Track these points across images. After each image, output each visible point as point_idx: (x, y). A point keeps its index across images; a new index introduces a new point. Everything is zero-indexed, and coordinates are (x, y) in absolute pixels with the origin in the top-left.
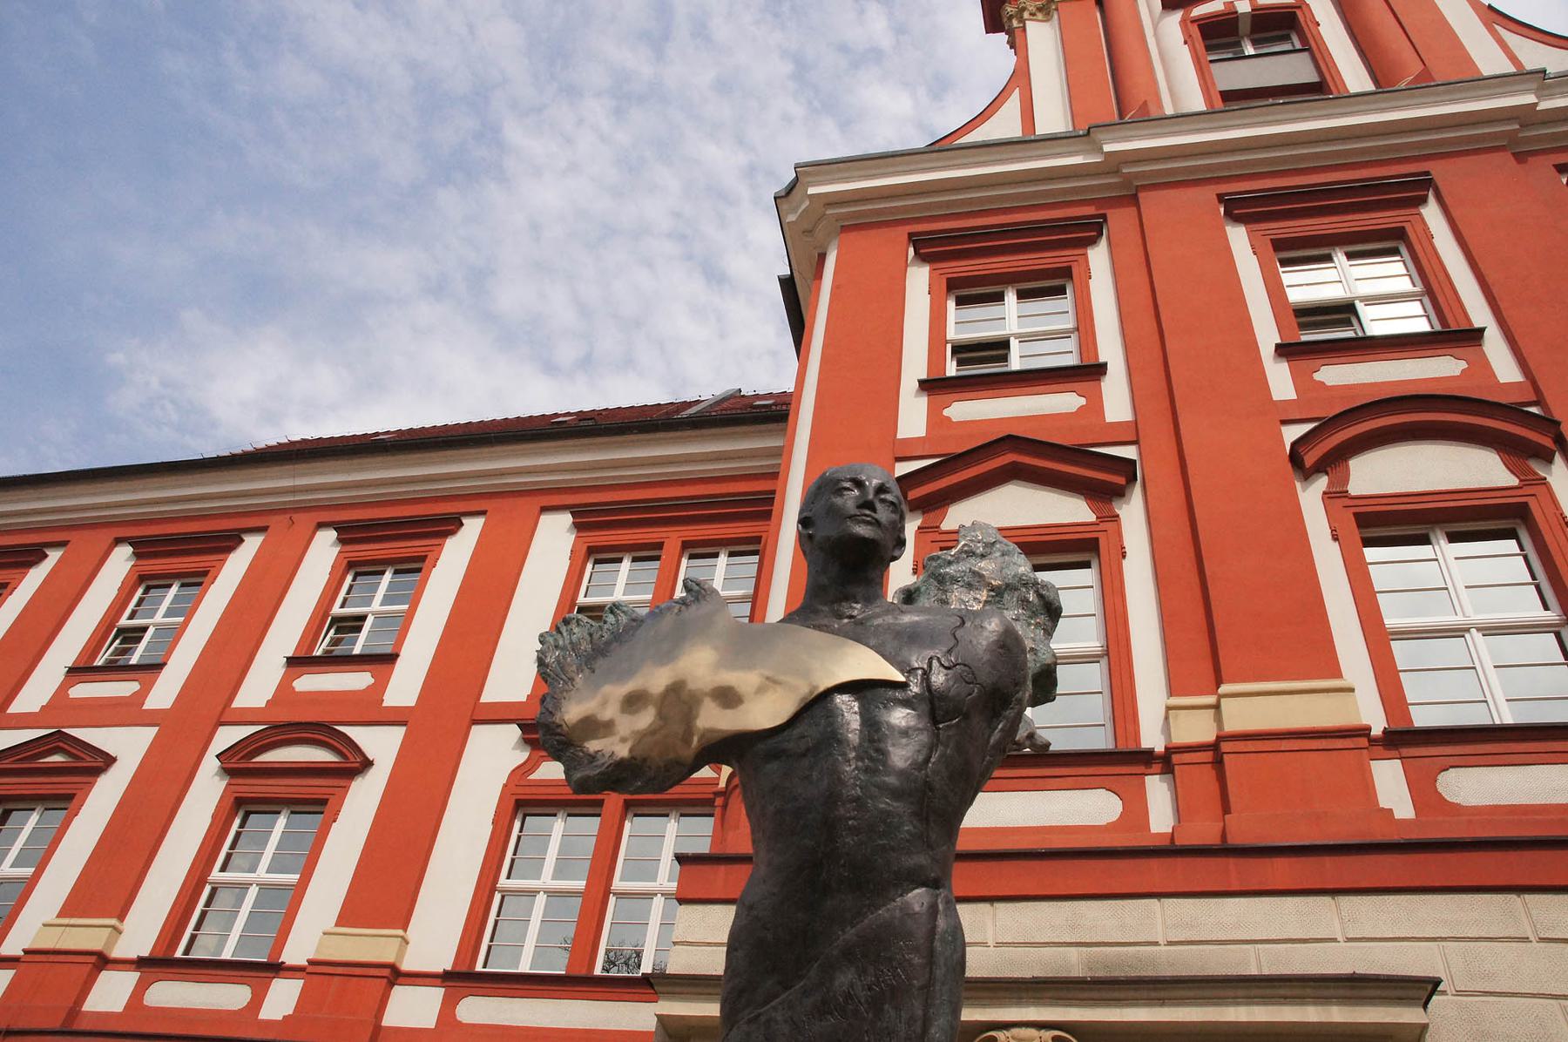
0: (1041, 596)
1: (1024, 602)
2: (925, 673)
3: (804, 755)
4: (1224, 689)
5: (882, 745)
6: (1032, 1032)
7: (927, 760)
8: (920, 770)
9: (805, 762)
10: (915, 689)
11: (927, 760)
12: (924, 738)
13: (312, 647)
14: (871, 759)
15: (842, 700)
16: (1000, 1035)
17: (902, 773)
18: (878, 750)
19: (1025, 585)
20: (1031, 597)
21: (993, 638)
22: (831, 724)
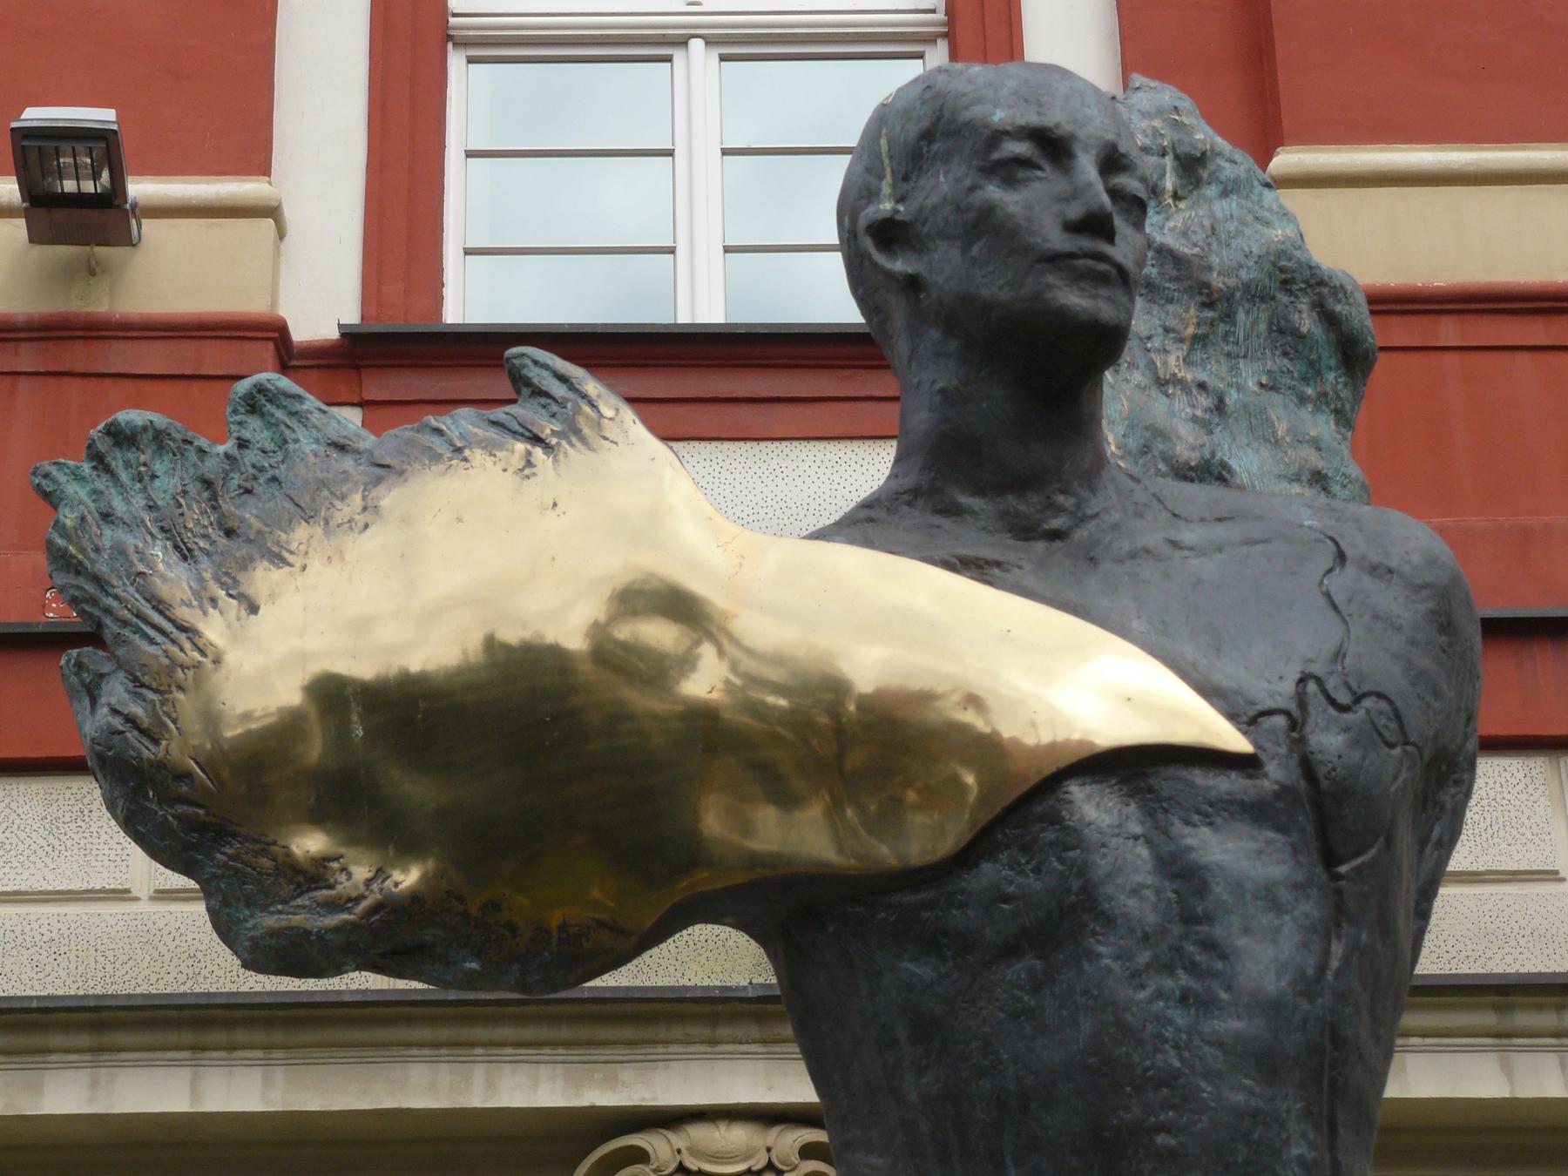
0: (1330, 319)
1: (1285, 336)
2: (1294, 725)
3: (1010, 951)
4: (1286, 160)
5: (1218, 932)
6: (737, 1136)
7: (1322, 968)
8: (1311, 996)
9: (1019, 970)
10: (1277, 772)
11: (1322, 968)
12: (1310, 908)
13: (192, 890)
14: (1193, 968)
15: (1077, 791)
16: (661, 1146)
17: (1275, 1008)
18: (1209, 945)
19: (1286, 284)
20: (1307, 322)
21: (880, 216)
22: (1082, 870)
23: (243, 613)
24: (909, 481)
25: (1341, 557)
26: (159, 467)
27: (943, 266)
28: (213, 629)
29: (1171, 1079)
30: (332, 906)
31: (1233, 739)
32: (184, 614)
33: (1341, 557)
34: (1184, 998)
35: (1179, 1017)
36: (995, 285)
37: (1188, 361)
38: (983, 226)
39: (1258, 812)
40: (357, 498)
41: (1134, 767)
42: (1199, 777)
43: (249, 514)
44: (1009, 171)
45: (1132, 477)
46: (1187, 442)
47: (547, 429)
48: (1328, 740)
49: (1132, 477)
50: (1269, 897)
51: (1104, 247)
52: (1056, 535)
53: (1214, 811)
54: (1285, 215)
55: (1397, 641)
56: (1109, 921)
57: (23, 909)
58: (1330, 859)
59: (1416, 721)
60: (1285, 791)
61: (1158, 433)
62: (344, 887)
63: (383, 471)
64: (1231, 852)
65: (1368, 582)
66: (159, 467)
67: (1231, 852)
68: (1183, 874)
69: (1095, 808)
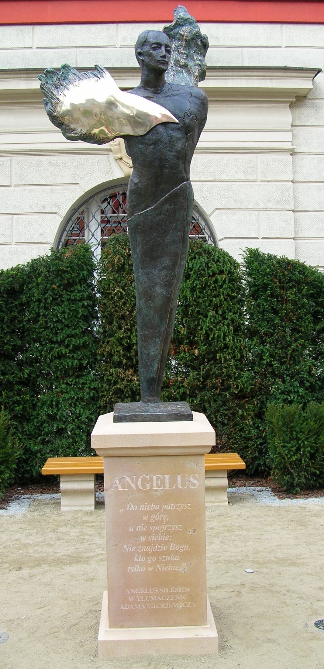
3: (151, 145)
12: (184, 140)
26: (53, 76)
27: (147, 59)
28: (60, 98)
30: (76, 134)
31: (177, 121)
32: (57, 96)
34: (169, 151)
35: (169, 153)
36: (153, 64)
37: (183, 50)
38: (150, 55)
39: (179, 129)
40: (77, 82)
43: (64, 83)
44: (154, 49)
46: (183, 62)
47: (99, 76)
50: (179, 139)
51: (165, 59)
53: (173, 129)
54: (198, 27)
55: (197, 107)
57: (14, 51)
58: (186, 134)
59: (198, 117)
60: (182, 127)
61: (179, 61)
62: (77, 132)
63: (80, 79)
65: (194, 99)
66: (53, 76)
67: (177, 134)
69: (161, 129)
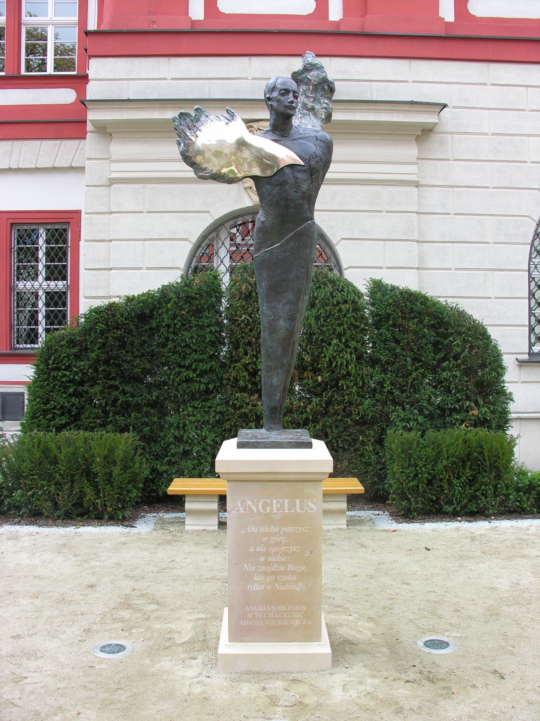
3: (277, 186)
12: (309, 182)
23: (181, 528)
24: (263, 153)
25: (317, 139)
26: (187, 118)
29: (293, 200)
33: (317, 139)
34: (295, 191)
36: (281, 109)
39: (304, 171)
41: (292, 166)
42: (299, 167)
45: (18, 681)
48: (313, 163)
49: (18, 681)
52: (286, 137)
53: (298, 171)
56: (288, 183)
57: (149, 81)
58: (311, 176)
59: (323, 159)
64: (300, 176)
66: (187, 118)
68: (297, 178)
